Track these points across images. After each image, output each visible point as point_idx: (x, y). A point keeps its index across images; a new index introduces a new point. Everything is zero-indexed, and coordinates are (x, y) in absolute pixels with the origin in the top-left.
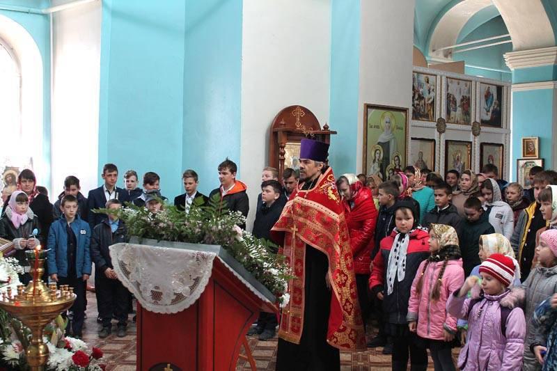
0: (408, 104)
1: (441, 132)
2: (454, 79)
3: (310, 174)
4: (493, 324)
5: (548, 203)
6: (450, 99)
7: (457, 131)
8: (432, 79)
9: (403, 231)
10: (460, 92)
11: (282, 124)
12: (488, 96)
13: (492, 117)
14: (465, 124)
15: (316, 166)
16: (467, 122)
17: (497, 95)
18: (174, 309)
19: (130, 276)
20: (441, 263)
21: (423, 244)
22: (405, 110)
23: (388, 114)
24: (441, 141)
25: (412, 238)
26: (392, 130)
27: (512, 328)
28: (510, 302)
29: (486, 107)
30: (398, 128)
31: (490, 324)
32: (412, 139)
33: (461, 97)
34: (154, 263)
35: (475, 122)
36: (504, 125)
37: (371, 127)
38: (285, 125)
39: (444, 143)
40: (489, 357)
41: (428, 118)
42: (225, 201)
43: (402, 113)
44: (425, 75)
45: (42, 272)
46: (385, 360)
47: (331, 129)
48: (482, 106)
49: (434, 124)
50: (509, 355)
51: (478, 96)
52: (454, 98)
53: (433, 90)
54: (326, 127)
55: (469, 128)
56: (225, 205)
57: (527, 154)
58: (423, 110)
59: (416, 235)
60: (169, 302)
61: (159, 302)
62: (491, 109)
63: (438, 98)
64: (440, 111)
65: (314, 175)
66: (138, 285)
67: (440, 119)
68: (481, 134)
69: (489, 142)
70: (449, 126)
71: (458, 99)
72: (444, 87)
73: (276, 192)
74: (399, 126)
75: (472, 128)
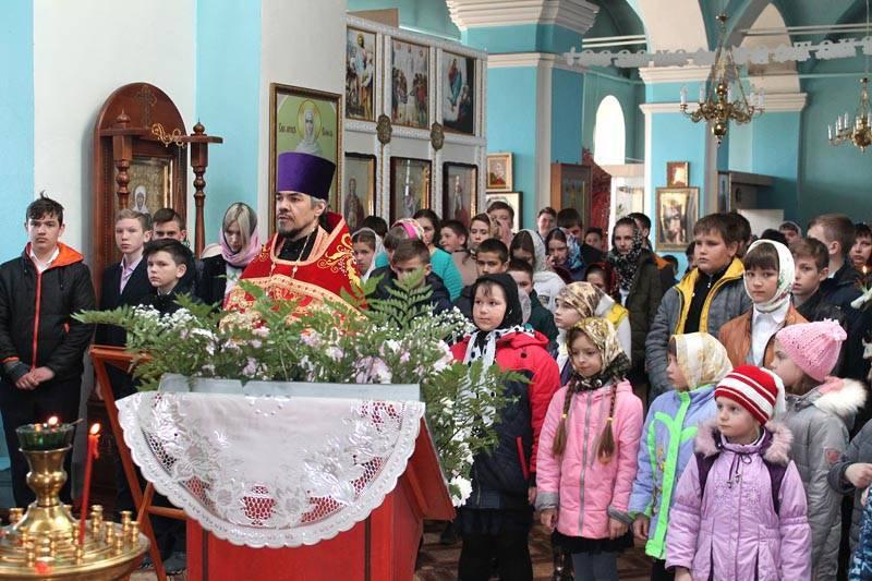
0: (338, 85)
1: (384, 140)
2: (414, 44)
3: (301, 223)
4: (759, 496)
5: (772, 271)
6: (397, 79)
7: (410, 141)
8: (368, 38)
9: (485, 327)
10: (412, 67)
11: (122, 121)
12: (453, 75)
13: (460, 114)
14: (420, 128)
15: (313, 207)
16: (423, 124)
17: (465, 74)
18: (309, 536)
19: (175, 467)
20: (606, 389)
21: (524, 356)
22: (334, 98)
23: (310, 104)
24: (384, 156)
25: (503, 345)
26: (317, 137)
27: (792, 499)
28: (780, 453)
29: (451, 96)
30: (326, 133)
31: (754, 496)
32: (347, 154)
33: (414, 77)
34: (253, 434)
35: (436, 123)
36: (477, 132)
37: (282, 130)
38: (127, 122)
39: (389, 162)
40: (757, 556)
41: (364, 115)
42: (430, 286)
43: (331, 103)
44: (358, 33)
45: (61, 481)
46: (450, 559)
47: (209, 132)
48: (446, 95)
49: (372, 127)
50: (796, 547)
51: (439, 75)
52: (403, 78)
53: (371, 61)
54: (199, 130)
55: (426, 134)
56: (429, 294)
57: (492, 183)
58: (354, 100)
59: (512, 340)
60: (292, 518)
61: (266, 523)
62: (459, 100)
63: (379, 77)
64: (382, 103)
65: (307, 225)
66: (199, 488)
67: (383, 116)
68: (444, 146)
69: (457, 161)
70: (396, 130)
71: (410, 80)
72: (388, 56)
73: (178, 264)
74: (327, 129)
75: (432, 135)
